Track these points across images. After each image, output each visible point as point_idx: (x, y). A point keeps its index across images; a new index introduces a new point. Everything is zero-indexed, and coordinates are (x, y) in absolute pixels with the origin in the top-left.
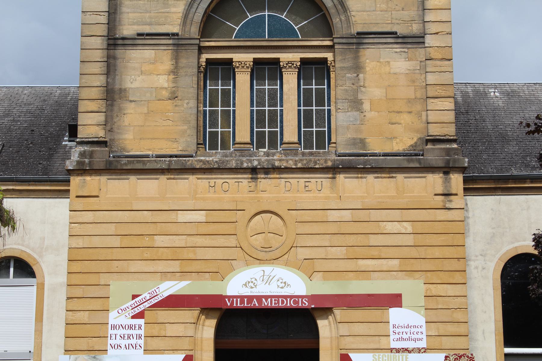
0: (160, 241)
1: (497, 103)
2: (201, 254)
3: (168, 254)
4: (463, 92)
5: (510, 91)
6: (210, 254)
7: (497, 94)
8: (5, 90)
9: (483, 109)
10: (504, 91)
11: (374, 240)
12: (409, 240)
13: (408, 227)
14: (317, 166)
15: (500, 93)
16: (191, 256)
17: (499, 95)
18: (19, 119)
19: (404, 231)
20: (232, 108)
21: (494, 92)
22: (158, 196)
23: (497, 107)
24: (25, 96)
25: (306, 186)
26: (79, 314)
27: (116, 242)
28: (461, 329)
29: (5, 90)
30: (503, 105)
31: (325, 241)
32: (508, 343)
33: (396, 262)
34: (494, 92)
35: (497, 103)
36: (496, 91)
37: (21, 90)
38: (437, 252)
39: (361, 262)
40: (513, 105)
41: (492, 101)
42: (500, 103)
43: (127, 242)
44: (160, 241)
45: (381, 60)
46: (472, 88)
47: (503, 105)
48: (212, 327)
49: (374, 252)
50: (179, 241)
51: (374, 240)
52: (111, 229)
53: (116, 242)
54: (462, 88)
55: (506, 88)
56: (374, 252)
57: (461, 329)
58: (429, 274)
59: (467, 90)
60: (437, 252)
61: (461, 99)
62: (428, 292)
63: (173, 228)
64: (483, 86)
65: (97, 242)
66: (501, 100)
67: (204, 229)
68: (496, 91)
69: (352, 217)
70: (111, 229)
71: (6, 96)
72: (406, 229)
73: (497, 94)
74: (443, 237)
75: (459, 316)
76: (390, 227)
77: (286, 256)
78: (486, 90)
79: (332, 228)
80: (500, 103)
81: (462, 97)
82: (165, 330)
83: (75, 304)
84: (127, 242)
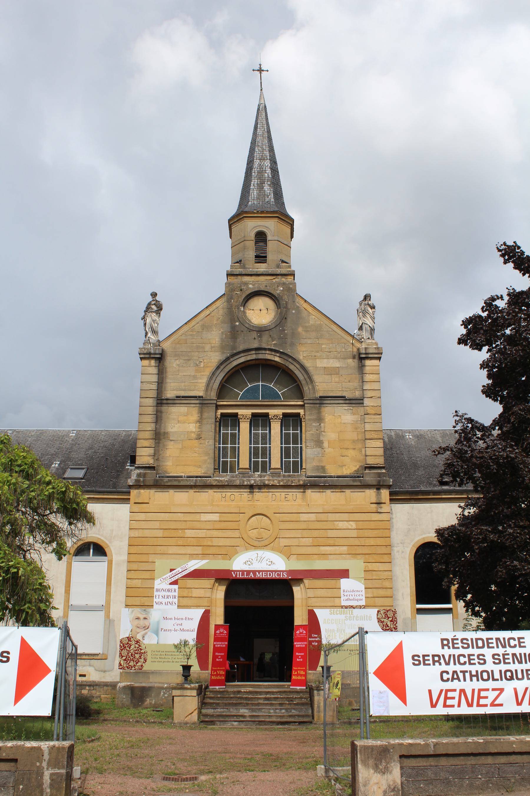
0: (189, 533)
2: (216, 542)
6: (222, 542)
7: (411, 437)
11: (331, 533)
12: (354, 533)
13: (353, 525)
16: (209, 543)
19: (350, 528)
21: (409, 435)
27: (160, 533)
28: (388, 593)
31: (298, 534)
33: (345, 548)
34: (409, 435)
38: (372, 542)
43: (167, 533)
44: (189, 533)
49: (331, 542)
51: (331, 533)
52: (157, 525)
53: (160, 533)
56: (331, 542)
60: (372, 542)
62: (366, 568)
65: (147, 533)
67: (218, 526)
70: (157, 525)
72: (352, 526)
73: (411, 437)
75: (387, 584)
76: (341, 525)
79: (304, 526)
82: (192, 593)
84: (167, 533)
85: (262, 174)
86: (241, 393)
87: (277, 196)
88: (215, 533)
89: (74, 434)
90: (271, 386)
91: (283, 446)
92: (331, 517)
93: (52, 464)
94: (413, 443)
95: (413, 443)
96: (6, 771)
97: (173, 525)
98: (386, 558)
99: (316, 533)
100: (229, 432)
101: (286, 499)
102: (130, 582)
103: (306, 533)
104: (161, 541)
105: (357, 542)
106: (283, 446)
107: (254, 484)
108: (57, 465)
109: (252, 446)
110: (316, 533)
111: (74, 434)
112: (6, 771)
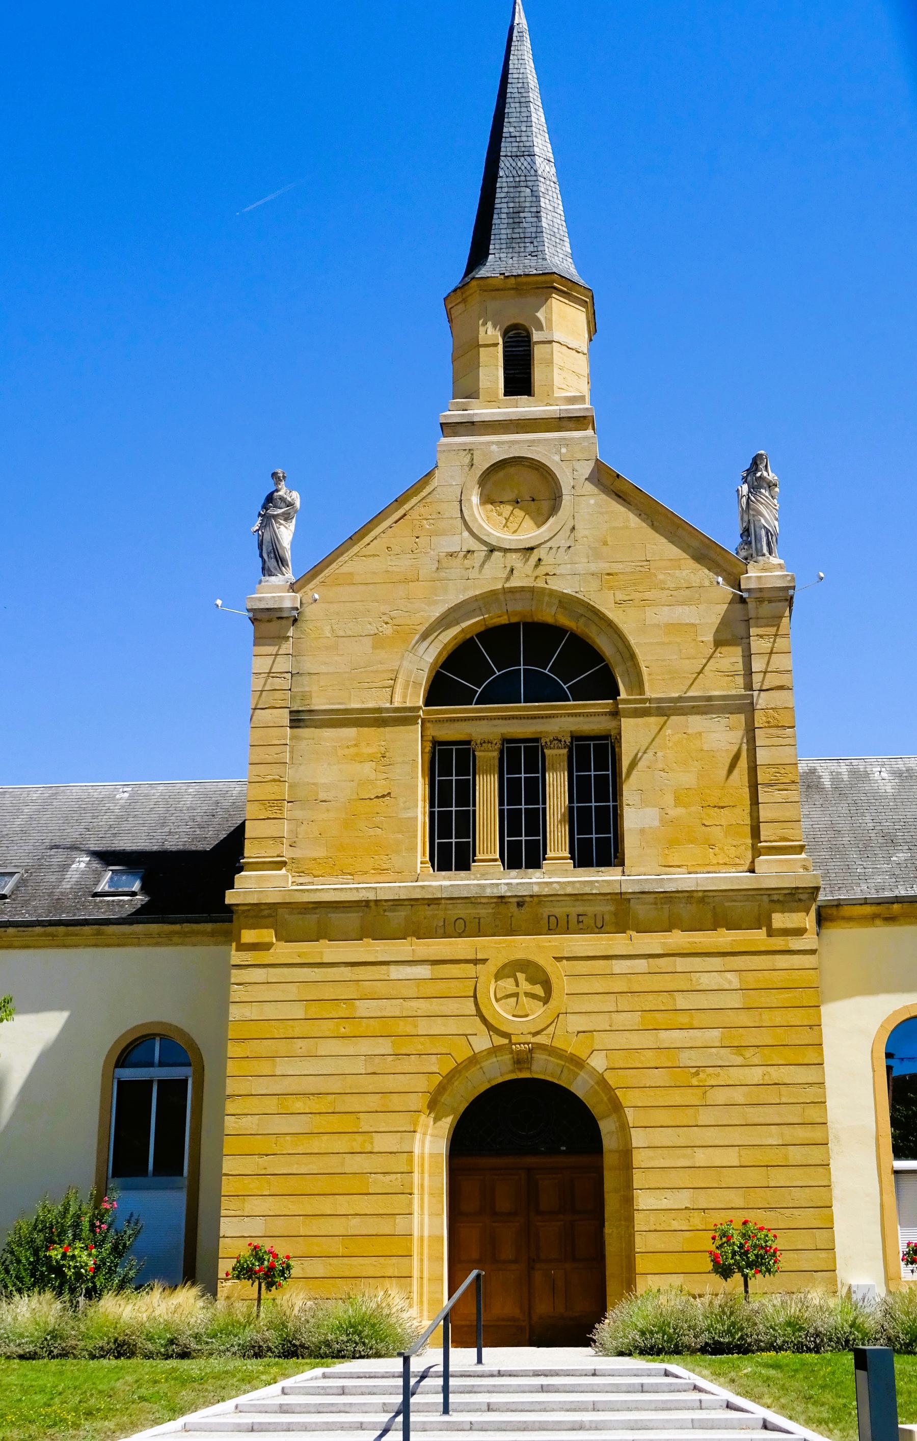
0: (363, 1008)
1: (883, 787)
2: (423, 1027)
3: (699, 1019)
4: (834, 773)
5: (904, 769)
6: (438, 1027)
7: (884, 775)
8: (161, 788)
9: (862, 798)
10: (895, 769)
11: (682, 1002)
12: (735, 1000)
13: (733, 980)
14: (594, 892)
15: (889, 772)
16: (410, 1030)
17: (886, 775)
18: (177, 830)
19: (727, 987)
20: (611, 804)
21: (880, 772)
22: (764, 929)
23: (884, 794)
24: (190, 796)
25: (579, 922)
26: (245, 1120)
27: (298, 1011)
28: (814, 1134)
29: (161, 788)
30: (893, 791)
31: (609, 1004)
32: (899, 1152)
33: (716, 1033)
34: (880, 772)
35: (883, 787)
36: (883, 769)
37: (185, 788)
38: (779, 1018)
39: (663, 1034)
40: (907, 790)
41: (876, 785)
42: (887, 787)
43: (314, 1011)
44: (363, 1008)
45: (690, 731)
46: (847, 767)
47: (893, 791)
48: (442, 1137)
49: (684, 1019)
50: (391, 1008)
51: (682, 1002)
52: (292, 992)
53: (298, 1011)
54: (833, 767)
55: (898, 766)
56: (684, 1019)
57: (814, 1134)
58: (766, 1051)
59: (840, 770)
60: (779, 1018)
61: (830, 783)
62: (766, 1077)
63: (381, 988)
64: (864, 763)
65: (271, 1012)
66: (890, 784)
67: (430, 989)
68: (883, 769)
69: (649, 966)
70: (292, 992)
71: (162, 797)
72: (730, 982)
73: (884, 775)
74: (786, 995)
75: (813, 1114)
76: (706, 981)
77: (552, 1028)
78: (867, 769)
79: (620, 986)
80: (887, 787)
81: (833, 780)
82: (372, 1143)
83: (810, 1094)
84: (314, 1011)
85: (518, 189)
86: (480, 691)
87: (553, 238)
88: (423, 1006)
89: (126, 795)
90: (546, 672)
91: (436, 809)
92: (681, 964)
93: (73, 862)
94: (889, 789)
95: (889, 789)
96: (711, 657)
97: (329, 992)
98: (811, 1057)
99: (651, 1002)
100: (454, 778)
101: (581, 926)
102: (236, 1123)
103: (624, 1003)
104: (298, 1029)
105: (744, 1019)
106: (436, 809)
107: (509, 894)
108: (83, 865)
109: (506, 807)
110: (651, 1002)
111: (126, 795)
112: (711, 657)
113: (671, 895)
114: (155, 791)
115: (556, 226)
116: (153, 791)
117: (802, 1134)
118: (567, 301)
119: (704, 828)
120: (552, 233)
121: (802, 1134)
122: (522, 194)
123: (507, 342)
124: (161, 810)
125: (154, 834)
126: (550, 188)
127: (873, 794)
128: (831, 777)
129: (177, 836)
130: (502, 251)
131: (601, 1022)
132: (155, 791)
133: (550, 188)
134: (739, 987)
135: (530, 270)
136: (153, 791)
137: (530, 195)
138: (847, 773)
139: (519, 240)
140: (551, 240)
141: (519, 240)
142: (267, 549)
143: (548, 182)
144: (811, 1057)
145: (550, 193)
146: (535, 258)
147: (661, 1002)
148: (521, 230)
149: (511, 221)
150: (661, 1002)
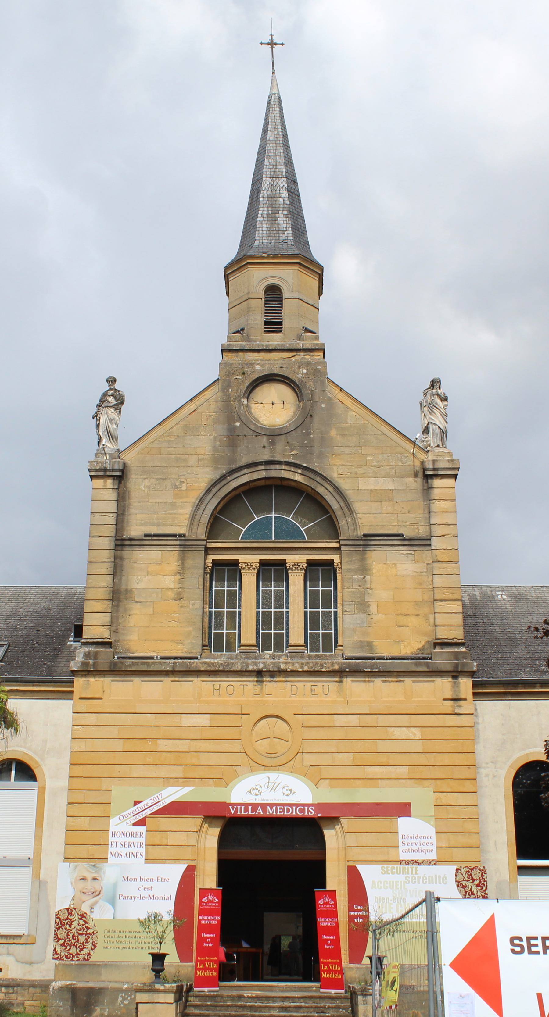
1: (505, 605)
2: (204, 759)
3: (394, 759)
5: (517, 593)
7: (505, 597)
9: (491, 612)
11: (382, 746)
12: (418, 746)
13: (417, 733)
14: (323, 670)
19: (412, 737)
20: (333, 610)
21: (502, 595)
26: (80, 819)
27: (119, 745)
28: (472, 840)
30: (511, 608)
31: (332, 747)
33: (405, 769)
34: (502, 595)
35: (505, 605)
37: (29, 590)
38: (446, 759)
39: (368, 769)
41: (500, 603)
42: (507, 605)
43: (129, 746)
45: (388, 562)
46: (479, 591)
47: (511, 608)
49: (383, 759)
50: (182, 746)
51: (382, 746)
52: (114, 732)
53: (119, 745)
54: (469, 591)
55: (513, 591)
56: (383, 759)
59: (474, 593)
60: (446, 759)
61: (468, 601)
64: (490, 589)
65: (99, 745)
66: (509, 603)
68: (504, 593)
70: (114, 732)
71: (13, 595)
72: (415, 734)
73: (505, 597)
75: (470, 826)
78: (493, 593)
79: (340, 734)
80: (507, 605)
84: (129, 746)
85: (275, 199)
86: (244, 530)
87: (297, 232)
95: (508, 606)
98: (468, 786)
104: (119, 758)
105: (423, 760)
107: (264, 670)
110: (359, 746)
113: (437, 972)
114: (8, 591)
115: (299, 224)
116: (7, 591)
117: (462, 840)
118: (306, 273)
119: (398, 628)
120: (297, 229)
121: (462, 840)
122: (277, 202)
123: (266, 298)
124: (13, 603)
125: (10, 621)
126: (295, 199)
127: (517, 614)
128: (469, 597)
129: (25, 623)
130: (264, 238)
131: (326, 759)
132: (8, 591)
133: (295, 199)
134: (420, 738)
135: (283, 251)
136: (7, 591)
137: (282, 203)
138: (479, 595)
139: (275, 232)
140: (296, 232)
141: (275, 232)
142: (102, 430)
143: (294, 196)
144: (468, 786)
145: (296, 203)
146: (286, 244)
147: (368, 746)
148: (276, 226)
149: (270, 219)
150: (368, 746)
